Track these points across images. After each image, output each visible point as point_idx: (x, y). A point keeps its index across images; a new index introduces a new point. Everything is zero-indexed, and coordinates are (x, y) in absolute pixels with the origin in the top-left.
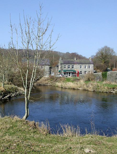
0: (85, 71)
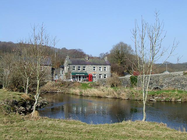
0: (100, 75)
